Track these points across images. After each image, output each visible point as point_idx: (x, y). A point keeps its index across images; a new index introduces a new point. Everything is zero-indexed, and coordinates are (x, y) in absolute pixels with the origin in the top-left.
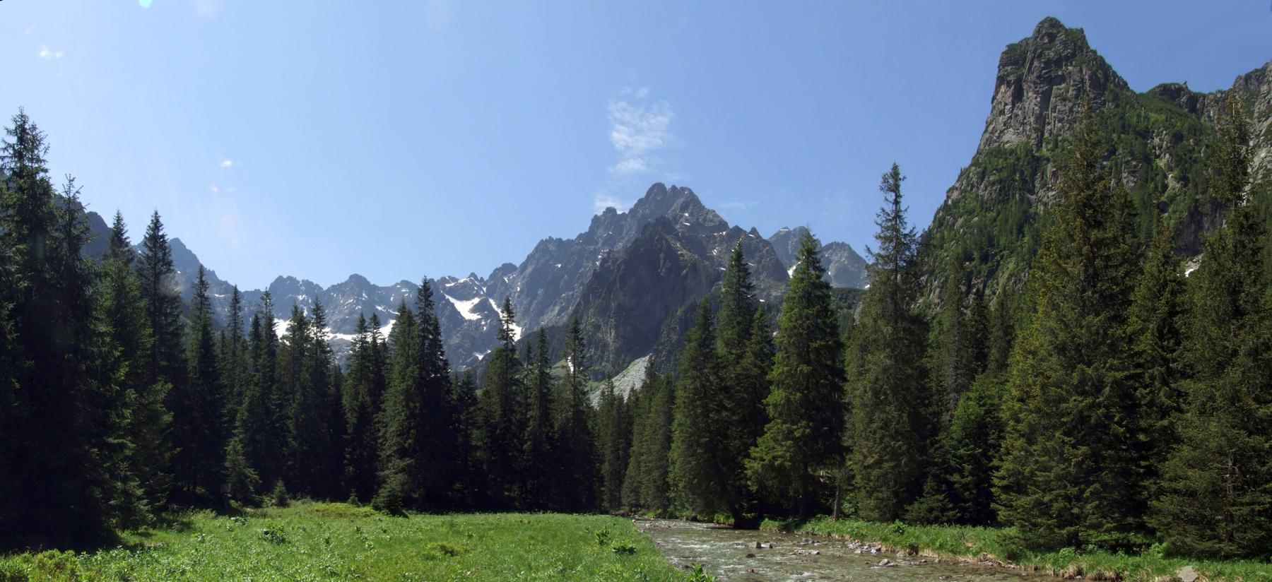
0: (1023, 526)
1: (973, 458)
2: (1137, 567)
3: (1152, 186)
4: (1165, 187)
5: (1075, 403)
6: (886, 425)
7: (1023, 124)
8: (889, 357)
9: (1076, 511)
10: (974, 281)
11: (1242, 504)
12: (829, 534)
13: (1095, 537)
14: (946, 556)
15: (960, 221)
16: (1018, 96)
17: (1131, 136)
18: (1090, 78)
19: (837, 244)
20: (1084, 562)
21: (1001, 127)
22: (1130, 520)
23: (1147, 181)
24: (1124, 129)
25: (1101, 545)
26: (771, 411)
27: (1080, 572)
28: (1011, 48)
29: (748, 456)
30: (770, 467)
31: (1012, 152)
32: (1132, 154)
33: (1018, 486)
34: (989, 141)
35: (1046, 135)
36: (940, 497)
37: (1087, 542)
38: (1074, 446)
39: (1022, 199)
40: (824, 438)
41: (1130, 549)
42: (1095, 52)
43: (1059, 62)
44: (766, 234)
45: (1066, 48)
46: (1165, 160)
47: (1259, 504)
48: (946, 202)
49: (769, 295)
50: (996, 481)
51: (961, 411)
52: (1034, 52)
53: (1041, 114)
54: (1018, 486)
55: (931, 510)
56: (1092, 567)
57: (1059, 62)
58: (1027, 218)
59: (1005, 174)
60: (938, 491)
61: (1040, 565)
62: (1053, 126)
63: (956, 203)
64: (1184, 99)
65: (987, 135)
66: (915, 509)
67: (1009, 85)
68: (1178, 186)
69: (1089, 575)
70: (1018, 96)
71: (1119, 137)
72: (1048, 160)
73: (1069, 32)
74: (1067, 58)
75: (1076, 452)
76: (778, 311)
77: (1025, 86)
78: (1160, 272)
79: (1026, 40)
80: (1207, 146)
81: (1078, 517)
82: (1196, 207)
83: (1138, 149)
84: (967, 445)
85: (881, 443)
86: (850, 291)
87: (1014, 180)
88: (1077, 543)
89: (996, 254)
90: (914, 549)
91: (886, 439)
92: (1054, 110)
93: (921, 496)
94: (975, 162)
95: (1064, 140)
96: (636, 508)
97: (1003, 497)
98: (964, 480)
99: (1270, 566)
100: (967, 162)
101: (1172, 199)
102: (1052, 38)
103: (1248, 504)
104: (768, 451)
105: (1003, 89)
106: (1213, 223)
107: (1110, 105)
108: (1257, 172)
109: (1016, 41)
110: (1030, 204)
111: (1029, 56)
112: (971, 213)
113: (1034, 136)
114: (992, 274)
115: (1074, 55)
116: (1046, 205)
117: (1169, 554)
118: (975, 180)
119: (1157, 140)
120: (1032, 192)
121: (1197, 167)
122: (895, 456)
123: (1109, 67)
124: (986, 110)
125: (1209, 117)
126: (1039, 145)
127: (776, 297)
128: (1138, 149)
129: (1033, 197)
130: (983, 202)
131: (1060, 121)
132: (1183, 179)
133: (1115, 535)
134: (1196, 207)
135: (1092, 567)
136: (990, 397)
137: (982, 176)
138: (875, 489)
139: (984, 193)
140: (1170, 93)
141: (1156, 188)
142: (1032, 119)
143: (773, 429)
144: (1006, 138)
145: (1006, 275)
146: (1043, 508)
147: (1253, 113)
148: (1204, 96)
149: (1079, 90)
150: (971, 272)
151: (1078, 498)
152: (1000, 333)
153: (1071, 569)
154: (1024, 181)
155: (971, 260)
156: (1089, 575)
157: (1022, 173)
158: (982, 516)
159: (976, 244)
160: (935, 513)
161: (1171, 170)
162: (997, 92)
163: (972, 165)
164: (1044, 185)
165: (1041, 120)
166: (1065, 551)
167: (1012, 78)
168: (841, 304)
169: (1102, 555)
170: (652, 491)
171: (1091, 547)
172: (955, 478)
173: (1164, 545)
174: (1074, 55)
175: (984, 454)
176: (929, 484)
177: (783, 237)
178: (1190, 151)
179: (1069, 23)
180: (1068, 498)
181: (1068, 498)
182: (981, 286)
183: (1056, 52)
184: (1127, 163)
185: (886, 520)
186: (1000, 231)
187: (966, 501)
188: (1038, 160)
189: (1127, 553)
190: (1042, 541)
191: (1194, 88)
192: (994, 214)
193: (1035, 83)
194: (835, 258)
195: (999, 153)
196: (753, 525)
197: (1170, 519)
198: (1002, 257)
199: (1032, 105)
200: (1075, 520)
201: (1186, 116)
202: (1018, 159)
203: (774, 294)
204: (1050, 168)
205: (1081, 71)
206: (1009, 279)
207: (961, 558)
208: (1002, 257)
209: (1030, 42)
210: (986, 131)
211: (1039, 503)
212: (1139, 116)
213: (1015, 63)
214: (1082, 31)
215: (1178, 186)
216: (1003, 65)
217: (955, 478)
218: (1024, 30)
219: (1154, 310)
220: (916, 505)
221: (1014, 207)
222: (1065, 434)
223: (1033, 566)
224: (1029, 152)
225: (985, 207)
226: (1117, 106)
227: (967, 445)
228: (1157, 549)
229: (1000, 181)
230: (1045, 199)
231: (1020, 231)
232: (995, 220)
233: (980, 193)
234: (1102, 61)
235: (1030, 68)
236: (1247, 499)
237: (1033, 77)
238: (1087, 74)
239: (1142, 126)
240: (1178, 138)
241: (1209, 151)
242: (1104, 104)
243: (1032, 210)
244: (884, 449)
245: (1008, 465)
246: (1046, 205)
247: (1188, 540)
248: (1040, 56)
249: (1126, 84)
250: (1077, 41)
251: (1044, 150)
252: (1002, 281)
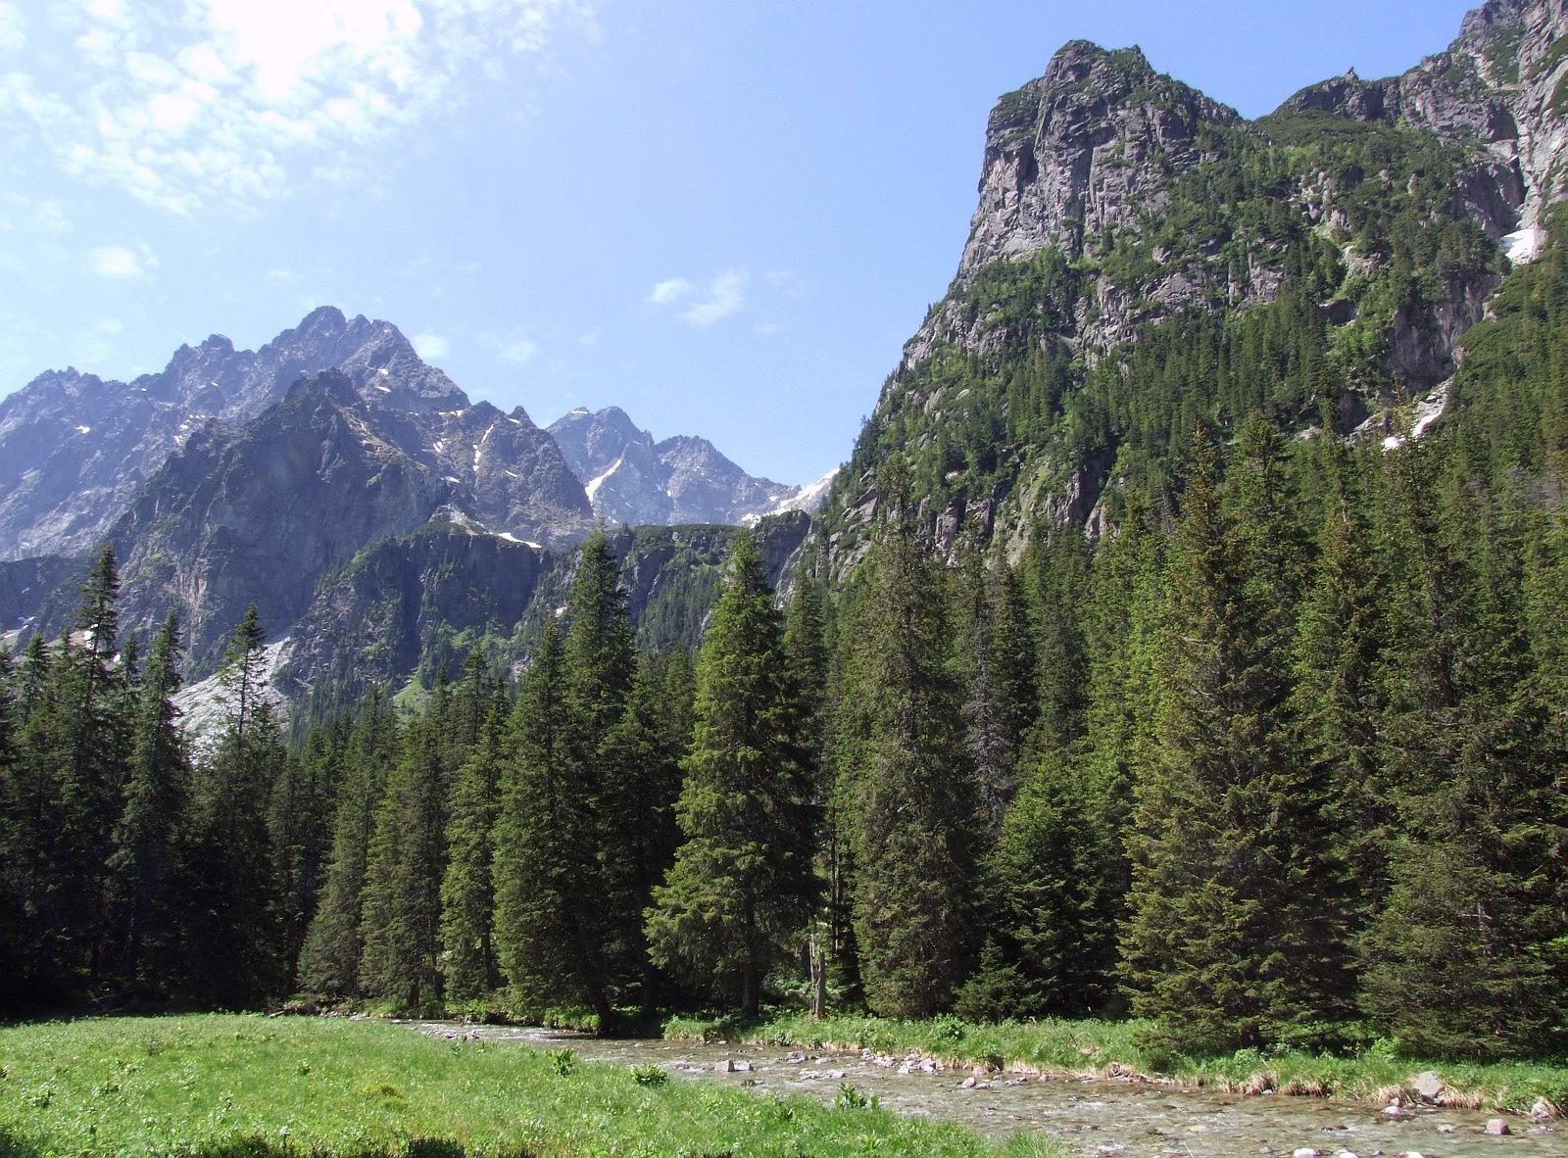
0: (1173, 1019)
1: (1053, 898)
2: (1351, 1074)
3: (1312, 277)
4: (1340, 273)
5: (1229, 842)
6: (911, 850)
7: (1041, 218)
8: (908, 746)
9: (1251, 993)
10: (970, 507)
11: (1498, 976)
12: (818, 1043)
13: (1287, 1030)
14: (1054, 1071)
15: (934, 398)
16: (1028, 173)
17: (1257, 201)
18: (1163, 121)
19: (685, 440)
20: (1274, 1069)
21: (1001, 228)
22: (1337, 1002)
23: (1299, 273)
24: (1241, 193)
25: (1295, 1043)
26: (686, 822)
27: (1268, 1085)
28: (1008, 100)
29: (653, 903)
30: (695, 925)
31: (1024, 268)
32: (1265, 231)
33: (1156, 959)
34: (979, 255)
35: (1089, 230)
36: (1010, 971)
37: (1275, 1041)
38: (1236, 900)
39: (1053, 349)
40: (787, 870)
41: (1339, 1047)
42: (1166, 78)
43: (1098, 109)
44: (543, 423)
45: (1110, 82)
46: (1331, 225)
47: (1528, 974)
48: (903, 365)
49: (545, 534)
50: (1124, 952)
51: (1021, 818)
52: (1052, 100)
53: (1074, 197)
54: (1156, 959)
55: (997, 994)
56: (1286, 1077)
57: (1098, 109)
58: (1065, 380)
59: (1014, 309)
60: (1002, 962)
61: (1207, 1078)
62: (1099, 213)
63: (923, 367)
64: (1353, 100)
65: (975, 245)
66: (970, 992)
67: (1008, 158)
68: (1368, 263)
69: (1283, 1089)
70: (1028, 173)
71: (1234, 208)
72: (1097, 272)
73: (1111, 57)
74: (1114, 99)
75: (1240, 908)
76: (567, 567)
77: (1039, 156)
78: (1337, 592)
79: (1035, 83)
80: (1420, 173)
81: (1255, 1001)
82: (1414, 294)
83: (1274, 220)
84: (1038, 875)
85: (904, 884)
86: (714, 530)
87: (1033, 316)
88: (1261, 1043)
89: (1010, 452)
90: (996, 1062)
91: (912, 879)
92: (1098, 186)
93: (978, 971)
94: (956, 293)
95: (1125, 233)
96: (346, 990)
97: (1137, 976)
98: (1038, 937)
99: (1563, 1072)
100: (939, 293)
101: (1359, 291)
102: (1082, 71)
103: (1507, 975)
104: (687, 894)
105: (998, 165)
106: (1459, 313)
107: (1209, 157)
108: (1548, 181)
109: (1014, 86)
110: (1069, 354)
111: (1043, 108)
112: (953, 382)
113: (1066, 235)
114: (1005, 488)
115: (1127, 91)
116: (1100, 351)
117: (1404, 1054)
118: (957, 322)
119: (1308, 194)
120: (1070, 331)
121: (1405, 216)
122: (928, 904)
123: (1197, 94)
124: (969, 204)
125: (1414, 113)
126: (1077, 250)
127: (561, 539)
128: (1274, 220)
129: (1073, 342)
130: (975, 361)
131: (1112, 202)
132: (1377, 248)
133: (1321, 1026)
134: (1414, 294)
135: (1286, 1077)
136: (1068, 789)
137: (971, 316)
138: (897, 962)
139: (976, 343)
140: (1321, 100)
141: (1321, 278)
142: (1059, 208)
143: (690, 860)
144: (1010, 246)
145: (1035, 490)
146: (1204, 993)
147: (1516, 68)
148: (1396, 81)
149: (1143, 145)
150: (963, 490)
151: (1251, 974)
152: (1060, 649)
153: (1255, 1080)
154: (1052, 314)
155: (961, 466)
156: (1283, 1089)
157: (1048, 302)
158: (1108, 1006)
159: (969, 438)
160: (1005, 1000)
161: (1347, 237)
162: (987, 172)
163: (949, 297)
164: (1093, 317)
165: (1076, 206)
166: (1241, 1054)
167: (1013, 147)
168: (697, 554)
169: (1297, 1057)
170: (391, 961)
171: (1280, 1046)
172: (1024, 933)
173: (1396, 1040)
174: (1127, 91)
175: (1069, 889)
176: (989, 950)
177: (577, 426)
178: (1383, 194)
179: (1110, 42)
180: (1236, 976)
181: (1236, 976)
182: (984, 515)
183: (1092, 94)
184: (1257, 249)
185: (916, 1015)
186: (1015, 409)
187: (1047, 974)
188: (1077, 275)
189: (1336, 1055)
190: (1201, 1040)
191: (1369, 74)
192: (1000, 380)
193: (1057, 149)
194: (680, 465)
195: (1001, 272)
196: (646, 1028)
197: (1398, 1000)
198: (1023, 457)
199: (1056, 185)
200: (1252, 1007)
201: (1363, 129)
202: (1038, 279)
203: (557, 532)
204: (1102, 287)
205: (1144, 113)
206: (1041, 497)
207: (1077, 1073)
208: (1023, 457)
209: (1042, 84)
210: (971, 238)
211: (1193, 983)
212: (1264, 160)
213: (1018, 122)
214: (1137, 49)
215: (1368, 263)
216: (995, 127)
217: (1024, 933)
218: (1027, 64)
219: (1337, 652)
220: (970, 986)
221: (1038, 365)
222: (1219, 881)
223: (1196, 1079)
224: (1058, 264)
225: (980, 369)
226: (1223, 155)
227: (1038, 875)
228: (1383, 1050)
229: (1007, 321)
230: (1098, 342)
231: (1056, 406)
232: (1003, 390)
233: (970, 344)
234: (1184, 88)
235: (1046, 125)
236: (1507, 966)
237: (1053, 140)
238: (1154, 116)
239: (1274, 176)
240: (1352, 176)
241: (1425, 181)
242: (1196, 156)
243: (1074, 365)
244: (906, 895)
245: (1139, 928)
246: (1100, 351)
247: (1426, 1033)
248: (1062, 105)
249: (1234, 113)
250: (1131, 71)
251: (1087, 255)
252: (1027, 501)
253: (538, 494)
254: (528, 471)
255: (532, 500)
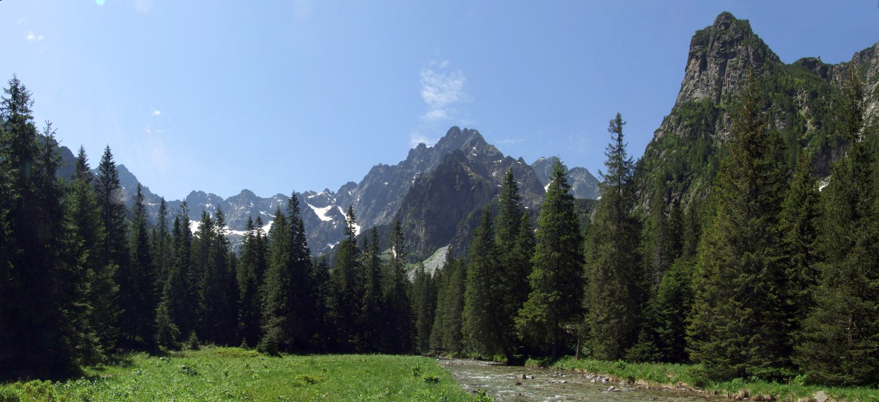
0: (707, 363)
1: (672, 317)
3: (796, 128)
4: (805, 129)
5: (743, 278)
6: (612, 294)
7: (707, 86)
8: (614, 247)
9: (743, 353)
10: (673, 194)
11: (858, 348)
12: (573, 369)
13: (757, 371)
14: (654, 384)
15: (664, 153)
16: (703, 66)
17: (782, 94)
18: (754, 54)
19: (579, 169)
20: (749, 388)
21: (692, 88)
22: (781, 359)
23: (792, 125)
24: (777, 89)
25: (761, 377)
26: (533, 284)
27: (746, 395)
28: (699, 33)
29: (517, 315)
30: (532, 323)
31: (699, 105)
32: (782, 106)
33: (703, 336)
34: (683, 98)
35: (723, 93)
36: (650, 343)
37: (751, 375)
38: (742, 308)
39: (706, 138)
40: (570, 303)
42: (756, 36)
43: (732, 43)
44: (529, 162)
45: (736, 33)
46: (805, 111)
47: (870, 348)
48: (654, 139)
49: (531, 204)
50: (688, 332)
51: (664, 284)
52: (715, 36)
53: (719, 79)
54: (703, 336)
55: (643, 352)
56: (755, 392)
57: (732, 43)
58: (709, 151)
59: (694, 120)
60: (648, 339)
61: (719, 390)
62: (728, 87)
63: (660, 140)
64: (818, 68)
65: (682, 93)
66: (632, 351)
67: (697, 59)
68: (814, 128)
69: (753, 397)
70: (703, 66)
71: (773, 95)
72: (724, 111)
73: (739, 22)
74: (738, 40)
75: (743, 312)
76: (538, 215)
77: (708, 60)
78: (802, 188)
79: (709, 28)
80: (834, 101)
81: (745, 357)
82: (827, 143)
83: (786, 103)
84: (668, 307)
85: (609, 306)
86: (587, 201)
87: (701, 125)
88: (744, 375)
89: (688, 176)
90: (632, 380)
91: (613, 303)
92: (728, 76)
93: (637, 343)
94: (674, 112)
95: (735, 97)
96: (440, 351)
97: (693, 343)
98: (666, 332)
99: (878, 391)
100: (668, 112)
101: (810, 137)
102: (727, 26)
103: (862, 348)
104: (531, 312)
105: (693, 61)
106: (838, 154)
107: (767, 73)
108: (869, 119)
109: (702, 28)
110: (712, 141)
111: (711, 38)
112: (671, 147)
113: (715, 94)
114: (685, 189)
115: (742, 38)
116: (723, 141)
117: (808, 383)
118: (674, 124)
119: (799, 97)
120: (713, 133)
121: (827, 115)
122: (619, 315)
123: (766, 46)
124: (681, 76)
125: (835, 80)
126: (718, 100)
127: (536, 205)
128: (786, 103)
129: (714, 136)
130: (679, 140)
131: (733, 83)
132: (818, 124)
133: (771, 370)
134: (827, 143)
135: (755, 392)
136: (684, 274)
137: (679, 122)
138: (605, 338)
139: (680, 133)
140: (809, 64)
141: (799, 130)
142: (713, 82)
143: (534, 296)
144: (695, 95)
145: (695, 190)
146: (721, 351)
147: (866, 78)
148: (832, 67)
149: (745, 62)
150: (671, 188)
151: (745, 344)
152: (691, 230)
153: (740, 393)
154: (708, 125)
155: (671, 179)
156: (753, 397)
157: (706, 120)
158: (678, 356)
159: (674, 168)
160: (646, 355)
161: (809, 117)
162: (689, 64)
163: (672, 114)
164: (721, 128)
165: (720, 83)
166: (736, 381)
167: (699, 54)
168: (581, 210)
169: (761, 383)
170: (451, 339)
171: (754, 378)
172: (660, 330)
173: (805, 376)
174: (742, 38)
175: (680, 314)
176: (642, 335)
177: (541, 164)
178: (823, 105)
179: (739, 16)
180: (738, 344)
181: (738, 344)
182: (678, 198)
183: (729, 36)
184: (779, 112)
185: (612, 359)
186: (691, 159)
187: (668, 346)
188: (717, 110)
189: (779, 382)
190: (720, 374)
191: (825, 61)
192: (687, 148)
193: (715, 57)
194: (577, 178)
195: (691, 105)
196: (520, 363)
197: (808, 358)
198: (692, 178)
199: (713, 73)
200: (743, 359)
201: (820, 80)
202: (703, 110)
203: (535, 203)
204: (726, 116)
205: (747, 49)
206: (697, 193)
207: (664, 386)
208: (692, 178)
209: (712, 29)
210: (681, 91)
211: (718, 348)
212: (787, 80)
213: (702, 44)
214: (748, 21)
215: (814, 128)
216: (693, 45)
217: (660, 330)
218: (707, 21)
219: (798, 214)
220: (633, 349)
221: (700, 143)
222: (736, 300)
223: (714, 391)
224: (711, 105)
225: (680, 143)
226: (772, 73)
227: (668, 307)
228: (799, 379)
229: (691, 125)
230: (722, 138)
231: (705, 160)
232: (688, 152)
233: (678, 133)
234: (762, 42)
235: (712, 47)
236: (862, 345)
237: (714, 53)
238: (751, 51)
239: (789, 87)
240: (814, 95)
241: (836, 104)
242: (763, 72)
243: (713, 145)
244: (611, 310)
245: (696, 321)
246: (723, 141)
247: (821, 373)
248: (718, 39)
249: (778, 58)
250: (744, 28)
251: (722, 103)
252: (692, 194)
253: (528, 189)
254: (525, 181)
255: (526, 192)
